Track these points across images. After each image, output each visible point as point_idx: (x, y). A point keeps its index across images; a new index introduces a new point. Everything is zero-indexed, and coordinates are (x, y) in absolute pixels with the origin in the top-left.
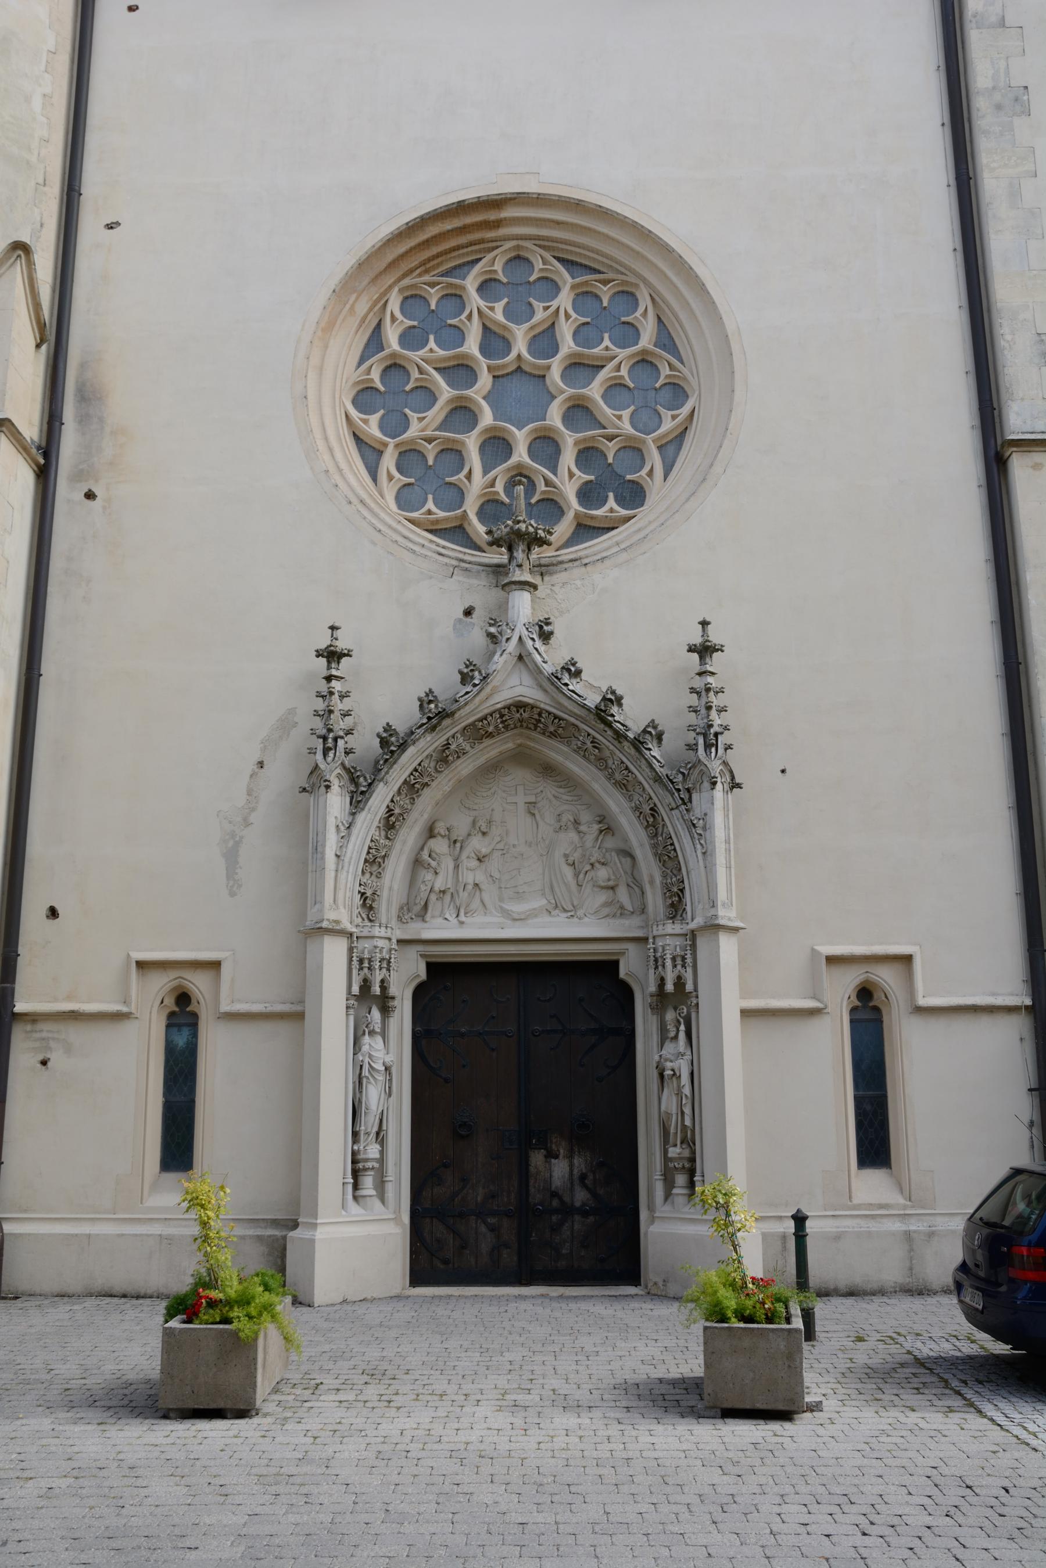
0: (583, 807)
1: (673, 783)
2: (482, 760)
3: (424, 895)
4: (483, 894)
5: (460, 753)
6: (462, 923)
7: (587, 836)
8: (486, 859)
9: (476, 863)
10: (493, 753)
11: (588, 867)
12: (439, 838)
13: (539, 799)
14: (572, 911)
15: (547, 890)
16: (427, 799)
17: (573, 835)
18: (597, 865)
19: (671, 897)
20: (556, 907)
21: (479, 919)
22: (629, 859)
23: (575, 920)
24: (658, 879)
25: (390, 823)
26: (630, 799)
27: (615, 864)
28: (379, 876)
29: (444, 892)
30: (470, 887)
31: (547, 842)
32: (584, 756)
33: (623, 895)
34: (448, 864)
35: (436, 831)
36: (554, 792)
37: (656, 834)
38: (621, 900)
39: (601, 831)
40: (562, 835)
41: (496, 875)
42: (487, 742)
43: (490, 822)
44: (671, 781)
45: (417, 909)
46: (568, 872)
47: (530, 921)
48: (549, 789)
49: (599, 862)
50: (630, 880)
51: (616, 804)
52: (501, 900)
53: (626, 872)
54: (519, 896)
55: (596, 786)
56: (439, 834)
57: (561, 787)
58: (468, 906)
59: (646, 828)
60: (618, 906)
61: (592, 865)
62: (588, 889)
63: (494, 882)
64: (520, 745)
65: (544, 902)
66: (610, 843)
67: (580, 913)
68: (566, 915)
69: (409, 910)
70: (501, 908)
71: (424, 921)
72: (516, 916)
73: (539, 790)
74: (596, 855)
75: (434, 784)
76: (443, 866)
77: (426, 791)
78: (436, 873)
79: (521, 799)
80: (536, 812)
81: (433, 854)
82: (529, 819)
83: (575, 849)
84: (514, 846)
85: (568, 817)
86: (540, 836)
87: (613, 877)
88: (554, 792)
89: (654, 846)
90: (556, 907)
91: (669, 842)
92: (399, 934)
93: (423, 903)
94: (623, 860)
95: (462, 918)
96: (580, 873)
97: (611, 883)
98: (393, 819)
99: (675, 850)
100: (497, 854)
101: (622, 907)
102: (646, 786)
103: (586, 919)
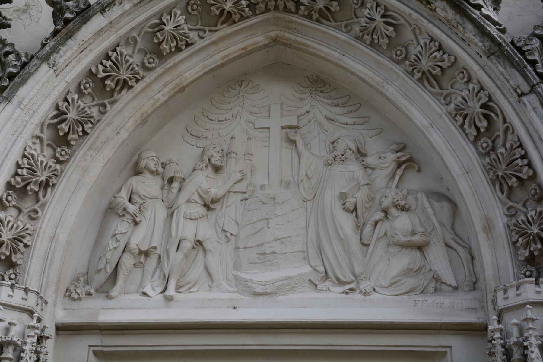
0: (372, 133)
1: (522, 53)
2: (215, 58)
3: (113, 257)
4: (209, 257)
5: (181, 44)
6: (169, 299)
7: (378, 172)
8: (217, 206)
9: (202, 210)
10: (234, 48)
11: (379, 215)
12: (147, 175)
13: (304, 121)
14: (351, 285)
15: (312, 252)
16: (126, 113)
17: (354, 168)
18: (393, 211)
19: (526, 245)
20: (326, 276)
21: (201, 294)
22: (446, 204)
23: (357, 296)
24: (500, 222)
25: (63, 133)
26: (447, 99)
27: (424, 209)
28: (33, 216)
29: (146, 254)
30: (187, 245)
31: (313, 182)
32: (372, 45)
33: (438, 260)
34: (155, 212)
35: (143, 164)
36: (326, 112)
37: (493, 149)
38: (435, 268)
39: (399, 165)
40: (337, 168)
41: (232, 229)
42: (225, 30)
43: (227, 155)
44: (519, 49)
45: (101, 278)
46: (347, 223)
47: (281, 298)
48: (319, 108)
49: (396, 206)
50: (449, 236)
51: (427, 117)
52: (237, 266)
53: (442, 224)
54: (266, 259)
55: (390, 90)
56: (147, 168)
57: (337, 105)
58: (183, 274)
59: (474, 142)
60: (430, 276)
61: (385, 212)
62: (379, 250)
63: (228, 240)
64: (275, 41)
65: (307, 269)
66: (413, 181)
67: (365, 285)
68: (341, 289)
69: (87, 283)
70: (236, 277)
71: (109, 298)
72: (258, 288)
73: (303, 111)
74: (391, 196)
75: (138, 87)
76: (148, 214)
77: (125, 96)
78: (136, 223)
79: (276, 123)
80: (298, 138)
81: (135, 198)
82: (287, 151)
83: (359, 186)
84: (262, 187)
85: (346, 143)
86: (303, 172)
87: (420, 229)
88: (326, 112)
89: (490, 168)
90: (326, 276)
91: (519, 152)
92: (63, 316)
93: (110, 269)
94: (437, 205)
95: (171, 291)
96: (365, 224)
97: (417, 239)
98: (64, 127)
99: (530, 165)
100: (234, 199)
101: (437, 279)
102: (474, 67)
103: (375, 296)
